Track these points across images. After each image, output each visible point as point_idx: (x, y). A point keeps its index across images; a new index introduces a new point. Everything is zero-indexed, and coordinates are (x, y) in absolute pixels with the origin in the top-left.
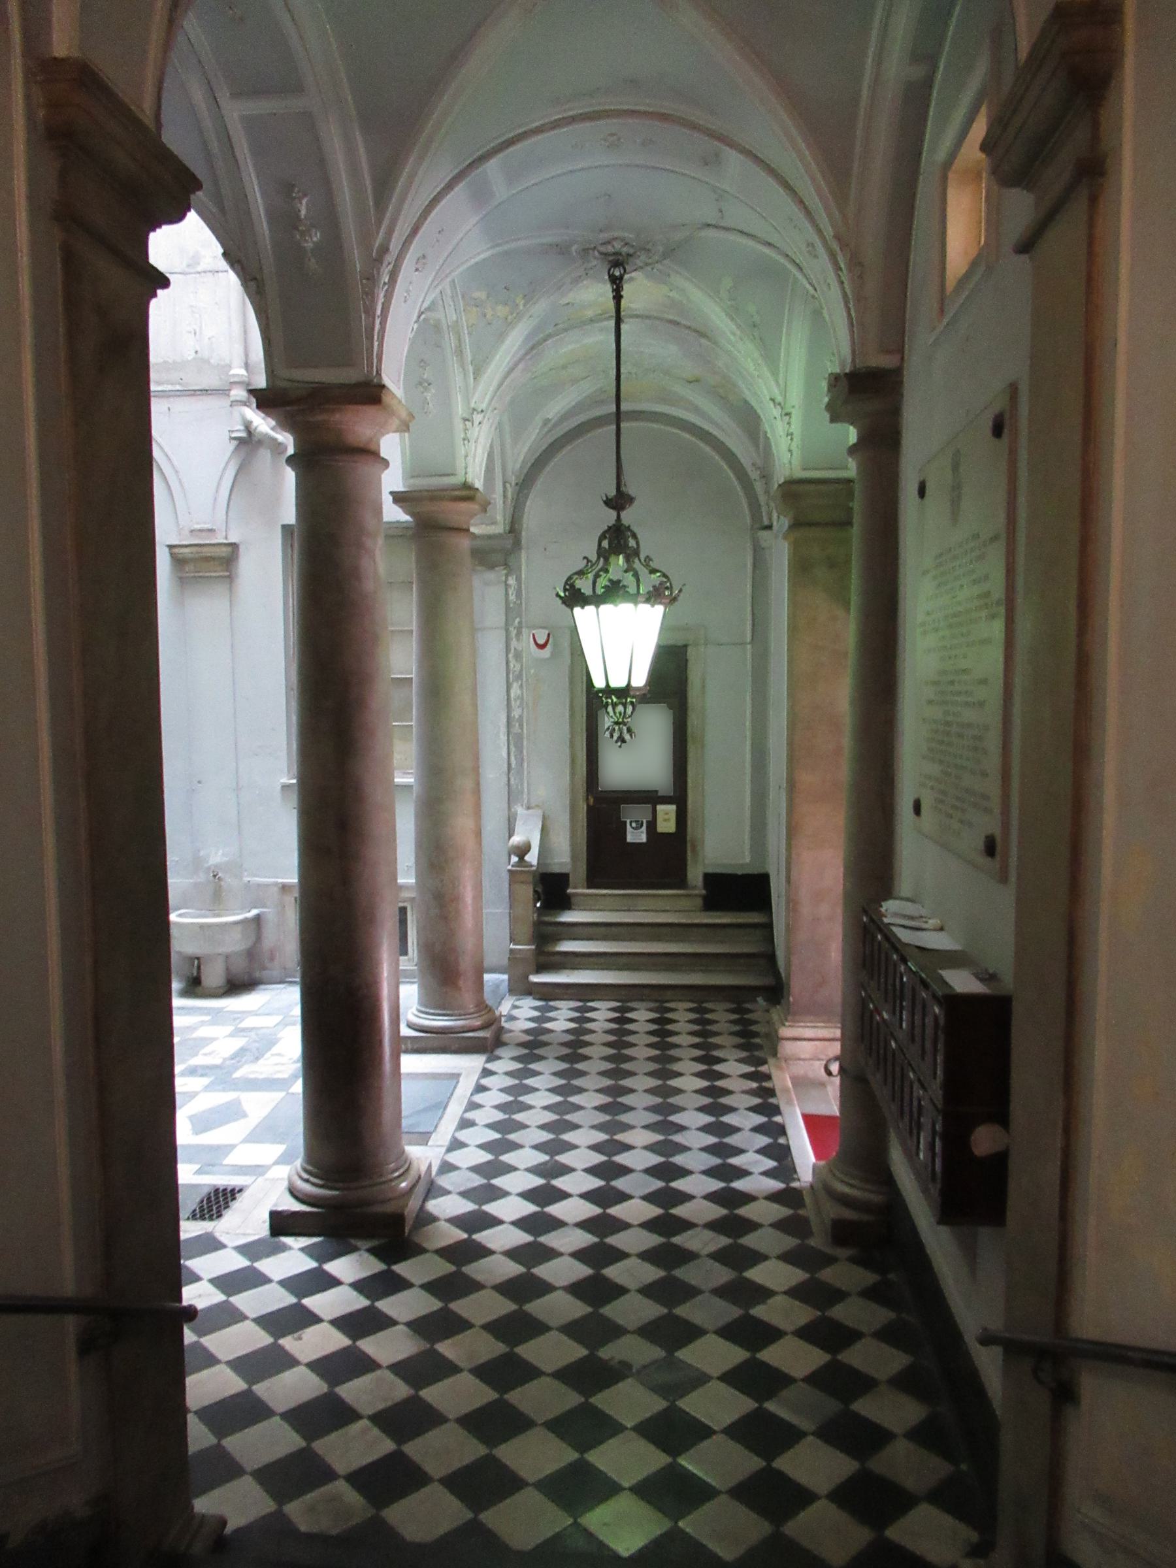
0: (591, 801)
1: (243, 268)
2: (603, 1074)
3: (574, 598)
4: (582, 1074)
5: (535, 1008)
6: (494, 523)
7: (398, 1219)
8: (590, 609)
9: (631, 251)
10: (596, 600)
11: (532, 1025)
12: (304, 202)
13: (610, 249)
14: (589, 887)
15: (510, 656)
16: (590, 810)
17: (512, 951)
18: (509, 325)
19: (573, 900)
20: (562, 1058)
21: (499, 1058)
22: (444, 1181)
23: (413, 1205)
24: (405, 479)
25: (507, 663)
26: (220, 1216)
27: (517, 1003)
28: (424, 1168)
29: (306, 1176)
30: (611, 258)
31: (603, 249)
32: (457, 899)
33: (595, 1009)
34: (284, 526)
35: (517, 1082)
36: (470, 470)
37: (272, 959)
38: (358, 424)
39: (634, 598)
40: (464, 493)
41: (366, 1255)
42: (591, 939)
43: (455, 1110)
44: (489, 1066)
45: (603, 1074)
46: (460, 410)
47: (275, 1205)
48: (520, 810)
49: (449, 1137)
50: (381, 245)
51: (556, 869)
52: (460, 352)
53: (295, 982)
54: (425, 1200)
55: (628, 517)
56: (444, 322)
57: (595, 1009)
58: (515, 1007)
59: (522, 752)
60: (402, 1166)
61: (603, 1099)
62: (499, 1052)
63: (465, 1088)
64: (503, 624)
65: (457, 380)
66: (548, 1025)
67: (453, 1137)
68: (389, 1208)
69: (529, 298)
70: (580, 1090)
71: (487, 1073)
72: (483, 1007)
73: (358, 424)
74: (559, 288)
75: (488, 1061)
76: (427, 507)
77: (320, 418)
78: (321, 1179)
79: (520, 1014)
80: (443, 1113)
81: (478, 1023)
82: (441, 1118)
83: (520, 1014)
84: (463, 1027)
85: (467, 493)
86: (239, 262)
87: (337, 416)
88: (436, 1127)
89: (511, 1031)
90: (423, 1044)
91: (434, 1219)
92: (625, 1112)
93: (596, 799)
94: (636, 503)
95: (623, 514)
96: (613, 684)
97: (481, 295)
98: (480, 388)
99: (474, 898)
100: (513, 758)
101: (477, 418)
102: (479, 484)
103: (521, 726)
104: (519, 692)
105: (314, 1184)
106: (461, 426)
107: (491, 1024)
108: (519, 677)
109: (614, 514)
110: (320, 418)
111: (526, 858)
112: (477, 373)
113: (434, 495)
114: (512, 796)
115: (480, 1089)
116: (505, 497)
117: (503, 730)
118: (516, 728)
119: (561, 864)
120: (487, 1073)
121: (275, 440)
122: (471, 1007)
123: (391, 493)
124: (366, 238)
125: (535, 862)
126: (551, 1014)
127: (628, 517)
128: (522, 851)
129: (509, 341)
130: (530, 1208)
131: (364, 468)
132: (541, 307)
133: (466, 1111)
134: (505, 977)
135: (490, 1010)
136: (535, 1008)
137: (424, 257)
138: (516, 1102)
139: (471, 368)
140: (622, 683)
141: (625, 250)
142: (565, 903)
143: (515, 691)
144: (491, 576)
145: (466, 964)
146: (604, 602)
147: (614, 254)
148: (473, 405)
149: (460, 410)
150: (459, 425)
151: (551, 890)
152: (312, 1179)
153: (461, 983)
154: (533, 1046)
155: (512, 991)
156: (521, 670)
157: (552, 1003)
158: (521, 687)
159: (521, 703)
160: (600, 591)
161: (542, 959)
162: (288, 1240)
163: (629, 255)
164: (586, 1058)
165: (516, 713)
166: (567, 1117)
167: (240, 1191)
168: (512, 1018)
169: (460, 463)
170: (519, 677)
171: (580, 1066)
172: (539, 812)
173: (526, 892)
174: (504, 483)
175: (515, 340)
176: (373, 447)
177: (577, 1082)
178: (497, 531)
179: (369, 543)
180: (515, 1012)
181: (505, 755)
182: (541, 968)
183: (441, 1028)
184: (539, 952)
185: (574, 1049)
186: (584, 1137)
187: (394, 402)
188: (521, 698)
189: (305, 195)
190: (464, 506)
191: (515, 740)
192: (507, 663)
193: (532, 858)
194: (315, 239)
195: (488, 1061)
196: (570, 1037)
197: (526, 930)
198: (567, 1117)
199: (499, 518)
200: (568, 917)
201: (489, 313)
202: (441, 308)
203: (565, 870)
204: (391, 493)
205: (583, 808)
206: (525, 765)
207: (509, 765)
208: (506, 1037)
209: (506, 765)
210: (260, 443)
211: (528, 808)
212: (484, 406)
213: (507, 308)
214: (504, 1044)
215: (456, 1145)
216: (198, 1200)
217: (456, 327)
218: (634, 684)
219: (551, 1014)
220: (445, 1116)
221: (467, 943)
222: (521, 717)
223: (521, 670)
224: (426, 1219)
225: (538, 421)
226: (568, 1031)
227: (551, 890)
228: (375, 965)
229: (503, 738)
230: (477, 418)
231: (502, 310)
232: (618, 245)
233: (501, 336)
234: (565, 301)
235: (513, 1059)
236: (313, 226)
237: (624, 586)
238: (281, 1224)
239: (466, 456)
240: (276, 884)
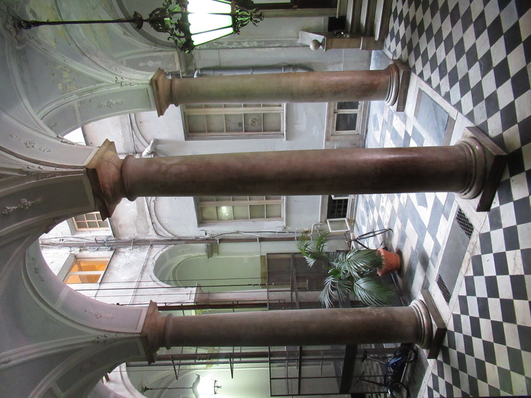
0: (295, 6)
1: (50, 225)
2: (433, 16)
3: (188, 45)
4: (431, 26)
5: (391, 40)
6: (173, 55)
7: (498, 159)
8: (193, 38)
9: (11, 18)
10: (188, 35)
11: (400, 44)
12: (9, 208)
13: (13, 30)
14: (336, 7)
15: (231, 47)
16: (300, 7)
17: (362, 49)
18: (72, 71)
19: (342, 15)
20: (420, 36)
21: (414, 66)
22: (479, 121)
23: (490, 145)
24: (152, 110)
25: (233, 48)
26: (471, 225)
27: (388, 47)
28: (470, 134)
29: (463, 194)
30: (18, 28)
31: (14, 34)
32: (337, 85)
33: (396, 8)
34: (186, 140)
35: (429, 62)
36: (144, 82)
37: (355, 144)
38: (109, 173)
39: (185, 15)
40: (154, 83)
41: (513, 178)
42: (361, 6)
43: (439, 99)
44: (418, 73)
45: (433, 16)
46: (117, 88)
47: (474, 208)
48: (299, 41)
49: (453, 109)
50: (19, 173)
51: (327, 23)
52: (91, 91)
53: (365, 106)
54: (487, 135)
55: (146, 17)
56: (78, 100)
57: (396, 8)
58: (389, 49)
59: (273, 41)
60: (468, 149)
61: (448, 20)
62: (411, 64)
63: (426, 88)
64: (217, 51)
65: (104, 90)
66: (401, 36)
67: (454, 106)
68: (490, 162)
69: (55, 63)
70: (440, 31)
71: (421, 75)
72: (388, 71)
73: (109, 173)
74: (46, 50)
75: (415, 73)
76: (163, 99)
77: (109, 193)
78: (466, 189)
79: (393, 49)
80: (439, 105)
81: (395, 74)
82: (442, 108)
83: (393, 49)
84: (396, 83)
85: (154, 83)
86: (48, 227)
87: (107, 186)
88: (447, 113)
89: (401, 55)
90: (402, 100)
91: (500, 137)
92: (458, 9)
93: (295, 4)
94: (139, 12)
95: (144, 18)
96: (230, 23)
97: (60, 86)
98: (107, 80)
99: (337, 76)
100: (275, 45)
101: (120, 80)
102: (151, 75)
103: (261, 41)
104: (246, 43)
105: (469, 192)
106: (125, 87)
107: (396, 66)
108: (239, 43)
109: (144, 23)
110: (109, 193)
111: (320, 41)
112: (99, 82)
113: (157, 98)
114: (292, 45)
115: (429, 82)
116: (161, 51)
117: (263, 50)
118: (263, 44)
119: (324, 21)
120: (421, 75)
121: (153, 144)
122: (388, 77)
123: (159, 116)
124: (17, 180)
125: (323, 37)
126: (396, 33)
127: (146, 17)
128: (317, 44)
129: (79, 69)
130: (485, 35)
131: (131, 166)
132: (59, 57)
133: (440, 94)
134: (373, 52)
135: (390, 67)
136: (391, 40)
137: (26, 144)
138: (440, 67)
139: (98, 85)
140: (230, 18)
141: (11, 22)
142: (343, 18)
143: (246, 44)
144: (196, 57)
145: (367, 80)
146: (189, 31)
147: (14, 26)
148: (115, 83)
149: (117, 88)
150: (125, 88)
151: (336, 28)
152: (465, 192)
153: (376, 83)
154: (410, 47)
155: (381, 48)
156: (237, 42)
157: (390, 30)
158: (244, 42)
159: (251, 41)
160: (182, 34)
161: (368, 33)
162: (493, 206)
163: (13, 18)
164: (422, 22)
165: (256, 44)
166: (455, 43)
167: (460, 210)
168: (395, 53)
169: (142, 87)
170: (239, 43)
171: (426, 27)
172: (300, 32)
173: (336, 41)
174: (155, 51)
175: (77, 66)
176: (119, 165)
177: (435, 31)
178: (177, 55)
179: (164, 168)
180: (392, 50)
181: (274, 49)
182: (372, 34)
183: (395, 93)
184: (364, 35)
185: (416, 27)
186: (469, 38)
187: (94, 163)
188: (249, 42)
189: (6, 208)
190: (160, 84)
191: (267, 44)
192: (233, 48)
193: (320, 38)
194: (26, 201)
195: (415, 73)
196: (409, 27)
197: (354, 41)
198: (455, 43)
199: (171, 53)
200: (350, 19)
201: (68, 80)
202: (71, 103)
203: (327, 18)
204: (159, 116)
205: (299, 11)
206: (279, 39)
207: (280, 47)
208: (404, 58)
209: (279, 48)
210: (155, 149)
211: (298, 38)
212: (114, 77)
213: (64, 73)
214: (408, 61)
215: (458, 106)
216: (461, 229)
217: (80, 94)
218: (229, 11)
219: (396, 33)
220: (441, 105)
221: (359, 78)
222: (257, 42)
223: (237, 42)
224: (499, 140)
225: (125, 38)
226: (406, 27)
227: (336, 28)
228: (366, 162)
229: (267, 50)
230: (120, 80)
231: (66, 75)
232: (10, 26)
233: (79, 74)
234: (53, 44)
235: (416, 60)
236: (20, 203)
237: (178, 21)
238: (484, 206)
239: (138, 84)
240: (325, 142)
